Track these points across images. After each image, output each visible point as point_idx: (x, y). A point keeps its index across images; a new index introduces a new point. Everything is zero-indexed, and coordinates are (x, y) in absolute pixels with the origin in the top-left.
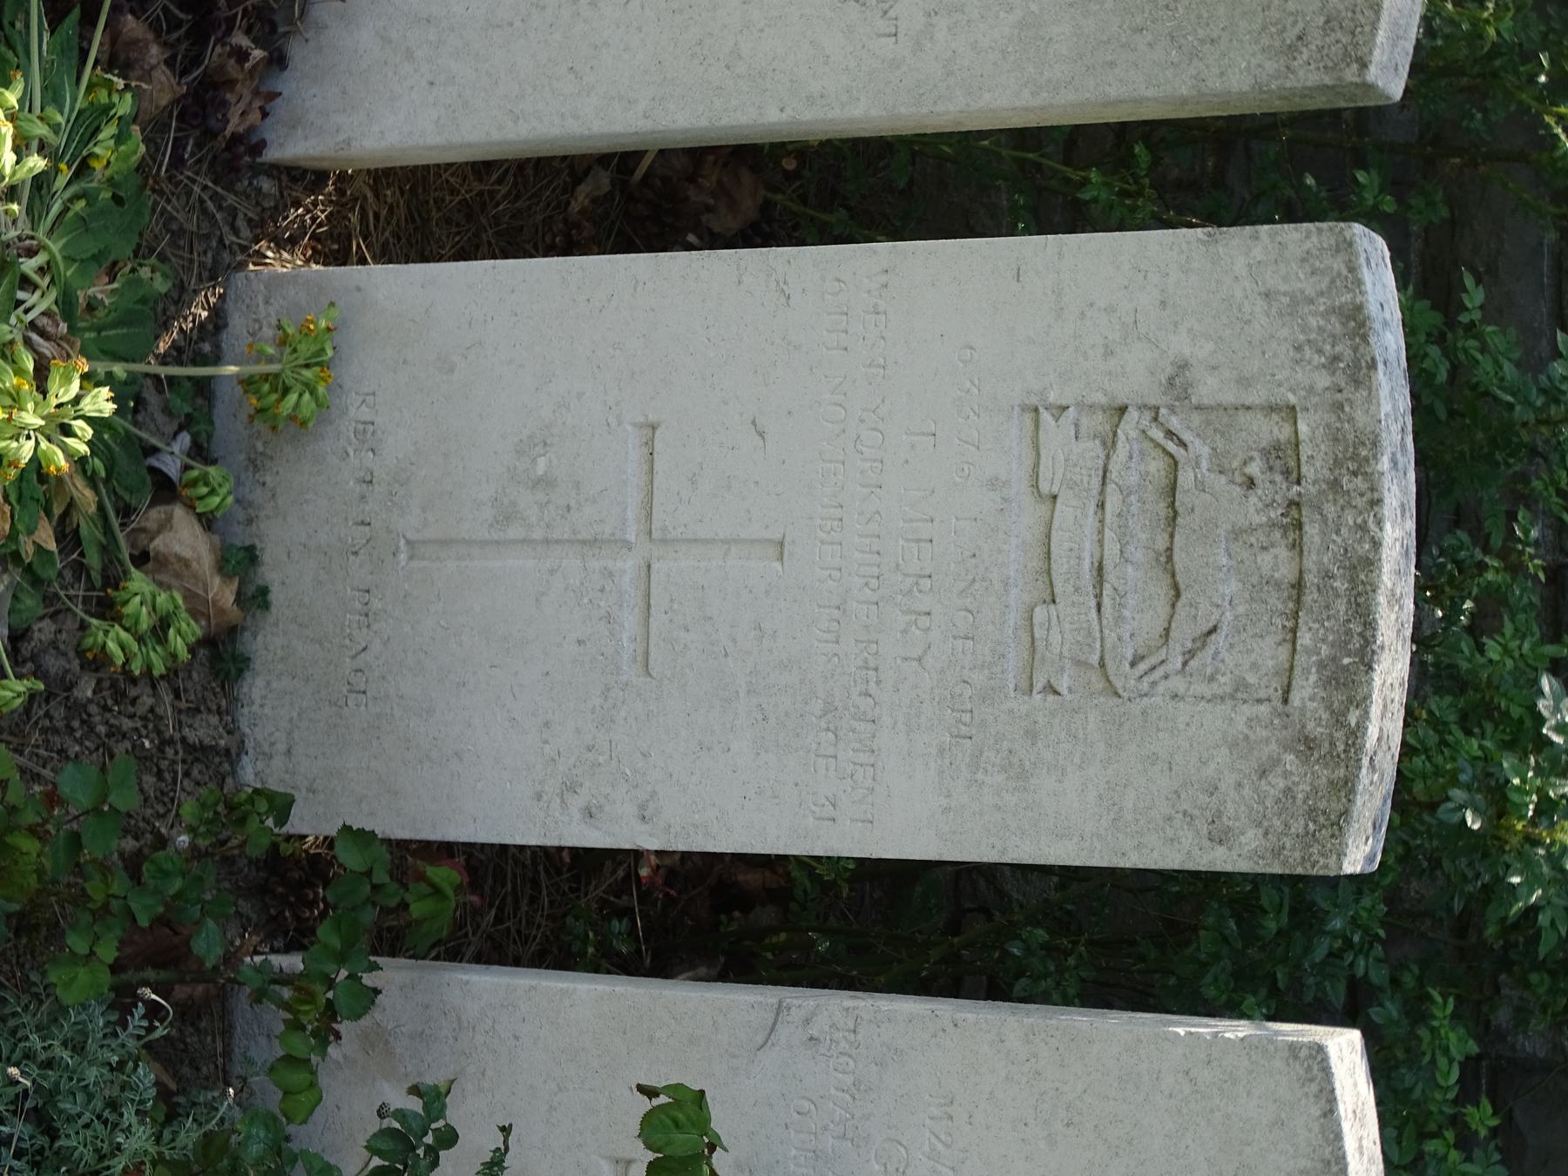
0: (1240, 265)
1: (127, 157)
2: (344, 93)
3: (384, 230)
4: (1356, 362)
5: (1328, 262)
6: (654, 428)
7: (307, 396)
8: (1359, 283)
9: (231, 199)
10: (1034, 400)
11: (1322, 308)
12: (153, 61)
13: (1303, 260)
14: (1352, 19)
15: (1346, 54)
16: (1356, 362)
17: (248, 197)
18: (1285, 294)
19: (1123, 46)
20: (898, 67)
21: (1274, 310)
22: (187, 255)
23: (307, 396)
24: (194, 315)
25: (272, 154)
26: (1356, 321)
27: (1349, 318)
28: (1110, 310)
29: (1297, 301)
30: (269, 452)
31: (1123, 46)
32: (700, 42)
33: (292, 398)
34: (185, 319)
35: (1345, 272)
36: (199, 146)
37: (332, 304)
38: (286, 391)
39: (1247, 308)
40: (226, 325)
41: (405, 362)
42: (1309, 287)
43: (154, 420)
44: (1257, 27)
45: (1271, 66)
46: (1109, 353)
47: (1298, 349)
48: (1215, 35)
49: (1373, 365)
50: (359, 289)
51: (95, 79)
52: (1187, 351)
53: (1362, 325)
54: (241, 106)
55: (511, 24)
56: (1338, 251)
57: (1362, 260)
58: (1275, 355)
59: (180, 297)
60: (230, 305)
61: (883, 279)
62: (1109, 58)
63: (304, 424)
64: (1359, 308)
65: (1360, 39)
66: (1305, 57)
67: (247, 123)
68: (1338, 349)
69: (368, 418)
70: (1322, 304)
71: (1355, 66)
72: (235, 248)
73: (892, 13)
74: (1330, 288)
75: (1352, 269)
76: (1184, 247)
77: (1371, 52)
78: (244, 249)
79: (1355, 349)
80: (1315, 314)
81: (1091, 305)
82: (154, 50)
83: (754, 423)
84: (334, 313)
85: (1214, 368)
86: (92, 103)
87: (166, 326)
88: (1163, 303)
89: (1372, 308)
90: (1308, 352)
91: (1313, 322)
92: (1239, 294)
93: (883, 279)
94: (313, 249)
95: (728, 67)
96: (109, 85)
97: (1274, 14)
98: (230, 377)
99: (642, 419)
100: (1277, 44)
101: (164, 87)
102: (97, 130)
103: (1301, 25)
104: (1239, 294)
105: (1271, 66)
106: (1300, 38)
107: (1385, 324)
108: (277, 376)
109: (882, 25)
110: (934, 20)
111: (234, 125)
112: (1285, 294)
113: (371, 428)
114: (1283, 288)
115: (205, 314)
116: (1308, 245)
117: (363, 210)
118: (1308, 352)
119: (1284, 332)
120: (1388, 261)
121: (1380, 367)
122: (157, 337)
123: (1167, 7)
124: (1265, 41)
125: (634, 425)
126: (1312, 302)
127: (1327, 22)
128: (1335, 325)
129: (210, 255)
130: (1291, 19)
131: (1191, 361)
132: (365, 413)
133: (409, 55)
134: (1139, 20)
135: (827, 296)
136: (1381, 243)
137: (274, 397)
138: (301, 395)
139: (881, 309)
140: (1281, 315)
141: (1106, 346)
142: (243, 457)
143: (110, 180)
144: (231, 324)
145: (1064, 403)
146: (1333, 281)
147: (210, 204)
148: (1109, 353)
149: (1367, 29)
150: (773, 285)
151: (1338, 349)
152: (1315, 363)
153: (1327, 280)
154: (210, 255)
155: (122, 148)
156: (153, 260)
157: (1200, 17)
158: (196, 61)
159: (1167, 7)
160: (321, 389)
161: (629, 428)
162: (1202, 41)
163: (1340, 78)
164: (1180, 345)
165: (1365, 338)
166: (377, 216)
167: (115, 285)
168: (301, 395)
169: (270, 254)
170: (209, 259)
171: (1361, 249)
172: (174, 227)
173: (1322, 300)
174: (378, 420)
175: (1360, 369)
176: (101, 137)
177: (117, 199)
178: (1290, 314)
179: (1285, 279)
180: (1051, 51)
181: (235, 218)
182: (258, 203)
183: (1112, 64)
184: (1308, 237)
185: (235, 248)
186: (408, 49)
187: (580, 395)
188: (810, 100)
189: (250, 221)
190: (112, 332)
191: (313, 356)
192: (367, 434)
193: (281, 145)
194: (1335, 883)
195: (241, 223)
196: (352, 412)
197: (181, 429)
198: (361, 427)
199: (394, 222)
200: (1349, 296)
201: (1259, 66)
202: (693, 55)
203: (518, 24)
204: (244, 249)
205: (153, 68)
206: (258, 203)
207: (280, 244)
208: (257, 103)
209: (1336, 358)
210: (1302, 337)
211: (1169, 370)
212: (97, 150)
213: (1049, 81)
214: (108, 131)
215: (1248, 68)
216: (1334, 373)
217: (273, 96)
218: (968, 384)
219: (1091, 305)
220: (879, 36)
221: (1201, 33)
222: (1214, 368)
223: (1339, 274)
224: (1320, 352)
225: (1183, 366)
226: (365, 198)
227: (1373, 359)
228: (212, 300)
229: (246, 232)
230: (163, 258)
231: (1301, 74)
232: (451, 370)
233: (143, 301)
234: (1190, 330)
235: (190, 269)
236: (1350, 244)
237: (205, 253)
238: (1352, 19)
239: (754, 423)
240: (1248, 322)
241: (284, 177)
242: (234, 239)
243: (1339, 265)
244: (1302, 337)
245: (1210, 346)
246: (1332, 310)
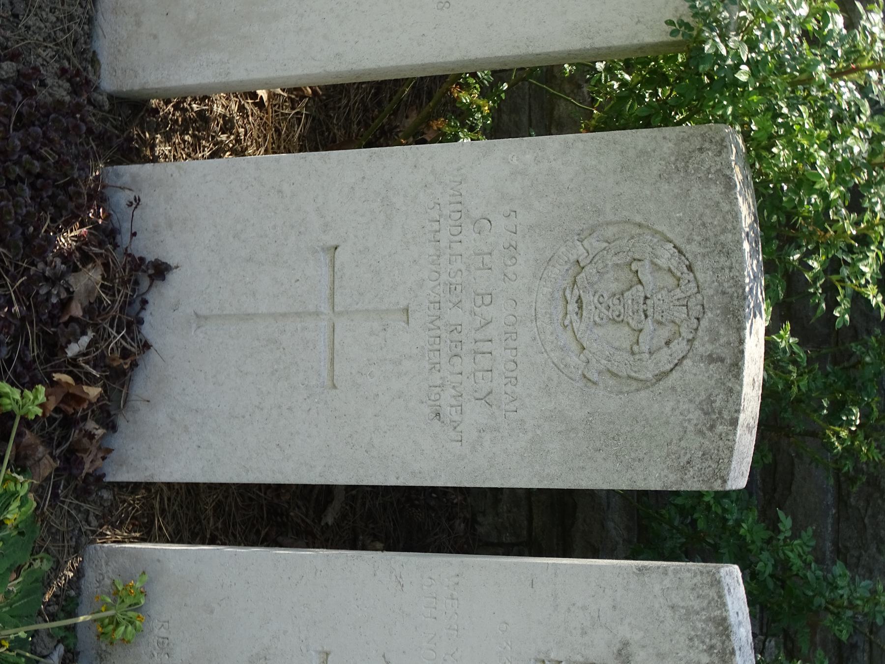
0: (657, 588)
1: (26, 512)
2: (150, 448)
3: (173, 504)
4: (724, 650)
5: (707, 591)
6: (327, 654)
7: (130, 628)
8: (724, 605)
9: (86, 506)
10: (542, 656)
11: (704, 618)
12: (40, 455)
13: (693, 589)
14: (717, 455)
15: (714, 474)
16: (724, 650)
17: (95, 503)
18: (683, 607)
19: (589, 458)
20: (463, 460)
21: (677, 616)
22: (61, 544)
23: (130, 628)
24: (65, 576)
25: (108, 479)
26: (723, 627)
27: (719, 624)
28: (584, 608)
29: (690, 612)
30: (109, 650)
31: (589, 458)
32: (351, 436)
33: (122, 628)
34: (60, 578)
35: (716, 598)
36: (68, 483)
37: (144, 573)
38: (118, 624)
39: (661, 614)
40: (84, 576)
41: (185, 605)
42: (697, 605)
43: (43, 641)
44: (664, 454)
45: (672, 477)
46: (584, 633)
47: (691, 639)
48: (641, 456)
49: (733, 653)
50: (159, 561)
51: (7, 476)
52: (628, 636)
53: (726, 629)
54: (91, 457)
55: (243, 417)
56: (712, 585)
57: (726, 591)
58: (678, 642)
59: (57, 568)
60: (86, 564)
61: (456, 580)
62: (581, 464)
63: (129, 642)
64: (725, 619)
65: (722, 466)
66: (691, 473)
67: (95, 467)
68: (714, 641)
69: (165, 635)
70: (704, 615)
71: (719, 481)
72: (89, 532)
73: (458, 429)
74: (708, 607)
75: (721, 596)
76: (625, 576)
77: (728, 474)
78: (93, 532)
79: (723, 643)
80: (700, 621)
81: (574, 604)
82: (41, 449)
83: (384, 656)
84: (145, 578)
85: (643, 647)
86: (5, 490)
87: (49, 586)
88: (614, 607)
89: (733, 619)
90: (696, 643)
91: (699, 625)
92: (657, 606)
93: (456, 580)
94: (134, 525)
95: (367, 452)
96: (16, 481)
97: (674, 448)
98: (84, 622)
99: (320, 649)
100: (676, 465)
101: (47, 466)
102: (9, 505)
103: (689, 456)
104: (657, 606)
105: (672, 477)
106: (688, 463)
107: (740, 623)
108: (113, 617)
109: (453, 434)
110: (483, 434)
111: (87, 468)
112: (683, 607)
113: (166, 641)
114: (682, 604)
115: (71, 574)
116: (695, 581)
117: (162, 499)
118: (696, 643)
119: (683, 630)
120: (741, 581)
121: (738, 653)
122: (44, 594)
123: (614, 438)
124: (669, 463)
125: (316, 651)
126: (698, 613)
127: (703, 455)
128: (711, 628)
129: (74, 540)
130: (683, 451)
131: (630, 641)
132: (163, 633)
133: (186, 429)
134: (598, 444)
135: (425, 587)
136: (736, 567)
137: (111, 627)
138: (126, 627)
139: (455, 597)
140: (681, 619)
141: (583, 629)
142: (94, 651)
143: (16, 527)
144: (86, 575)
145: (560, 660)
146: (709, 603)
147: (73, 512)
148: (584, 633)
149: (726, 461)
150: (394, 578)
151: (714, 641)
152: (701, 648)
153: (706, 602)
154: (74, 540)
155: (23, 509)
156: (42, 554)
157: (632, 446)
158: (65, 438)
159: (614, 438)
160: (138, 623)
161: (313, 653)
162: (634, 460)
163: (711, 487)
164: (624, 631)
165: (728, 636)
166: (169, 499)
167: (20, 579)
168: (126, 627)
169: (108, 533)
170: (73, 543)
171: (725, 585)
172: (54, 530)
173: (704, 613)
174: (171, 637)
175: (726, 654)
176: (11, 508)
177: (21, 534)
178: (686, 619)
179: (683, 599)
180: (549, 458)
181: (88, 516)
182: (101, 505)
183: (583, 468)
184: (695, 576)
185: (89, 532)
186: (185, 426)
187: (285, 632)
188: (413, 473)
189: (96, 516)
190: (17, 604)
191: (132, 602)
192: (164, 645)
193: (114, 475)
194: (727, 494)
195: (92, 518)
196: (156, 631)
197: (59, 642)
198: (161, 640)
199: (179, 499)
200: (719, 612)
201: (666, 476)
202: (347, 443)
203: (247, 417)
204: (93, 532)
205: (40, 460)
206: (101, 505)
207: (113, 527)
208: (100, 455)
209: (712, 647)
210: (693, 633)
211: (618, 646)
212: (8, 516)
213: (548, 475)
214: (15, 505)
215: (660, 477)
216: (711, 655)
217: (109, 451)
218: (505, 644)
219: (574, 604)
220: (452, 441)
221: (633, 455)
222: (643, 647)
223: (713, 599)
224: (703, 642)
225: (626, 644)
226: (162, 490)
227: (733, 649)
228: (76, 565)
229: (94, 523)
230: (47, 551)
231: (689, 483)
232: (212, 612)
233: (36, 580)
234: (630, 624)
235: (63, 551)
236: (719, 582)
237: (71, 538)
238: (717, 455)
239: (384, 656)
240: (662, 622)
241: (116, 489)
242: (88, 528)
243: (712, 593)
244: (693, 633)
245: (641, 634)
246: (709, 619)
